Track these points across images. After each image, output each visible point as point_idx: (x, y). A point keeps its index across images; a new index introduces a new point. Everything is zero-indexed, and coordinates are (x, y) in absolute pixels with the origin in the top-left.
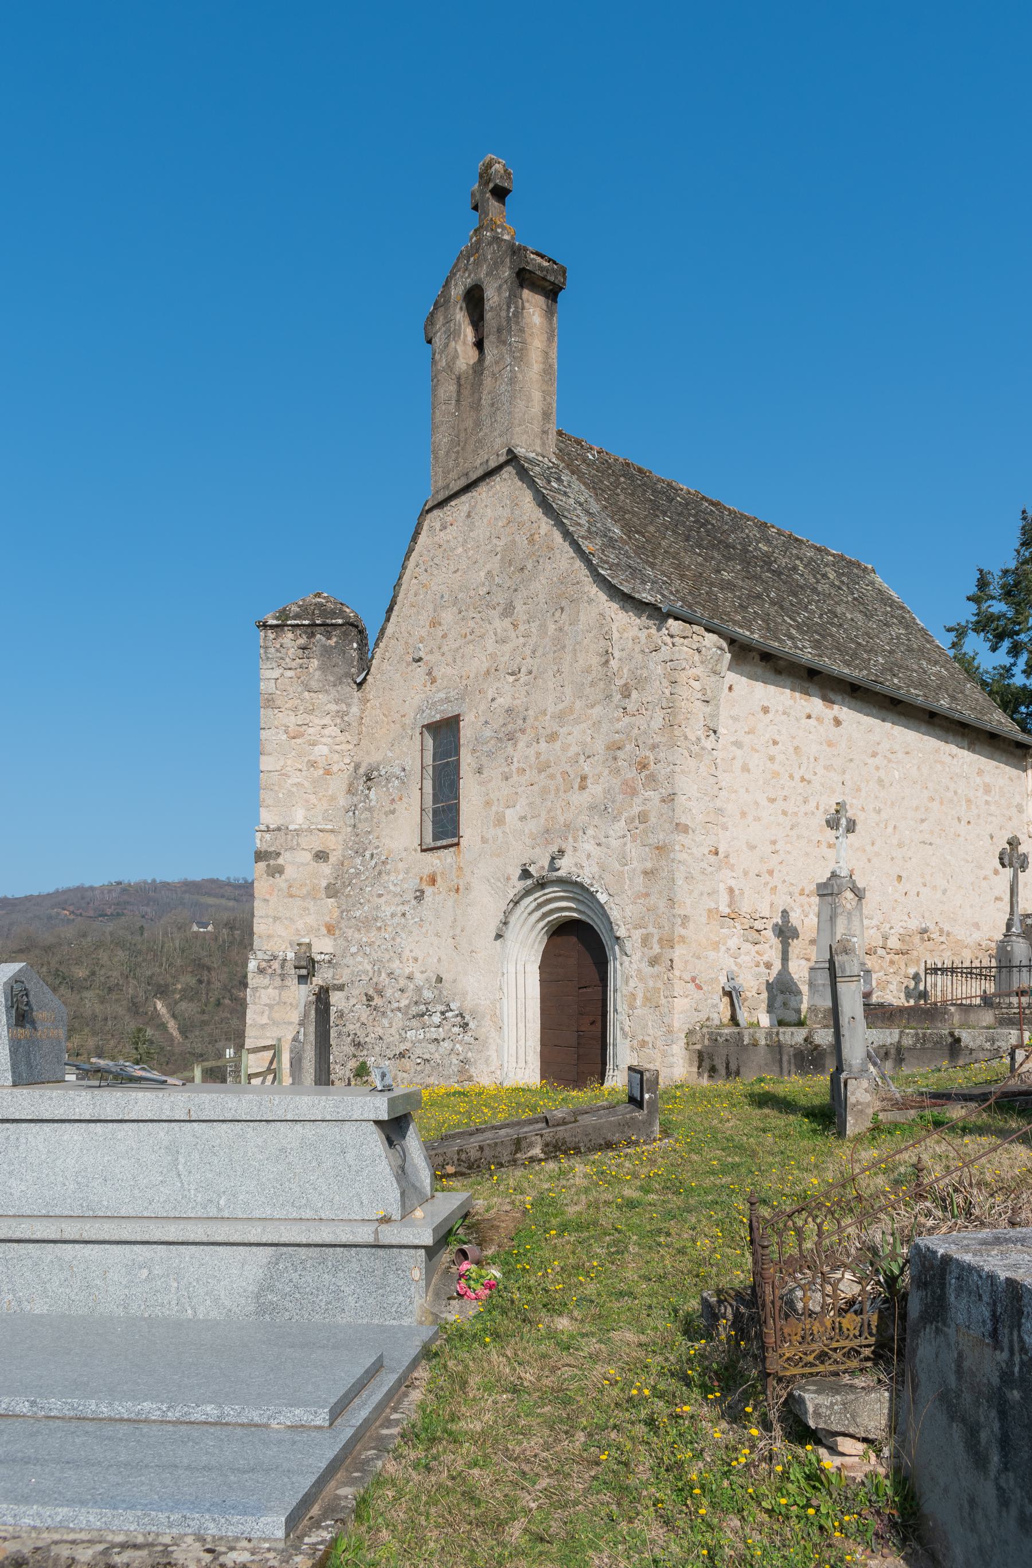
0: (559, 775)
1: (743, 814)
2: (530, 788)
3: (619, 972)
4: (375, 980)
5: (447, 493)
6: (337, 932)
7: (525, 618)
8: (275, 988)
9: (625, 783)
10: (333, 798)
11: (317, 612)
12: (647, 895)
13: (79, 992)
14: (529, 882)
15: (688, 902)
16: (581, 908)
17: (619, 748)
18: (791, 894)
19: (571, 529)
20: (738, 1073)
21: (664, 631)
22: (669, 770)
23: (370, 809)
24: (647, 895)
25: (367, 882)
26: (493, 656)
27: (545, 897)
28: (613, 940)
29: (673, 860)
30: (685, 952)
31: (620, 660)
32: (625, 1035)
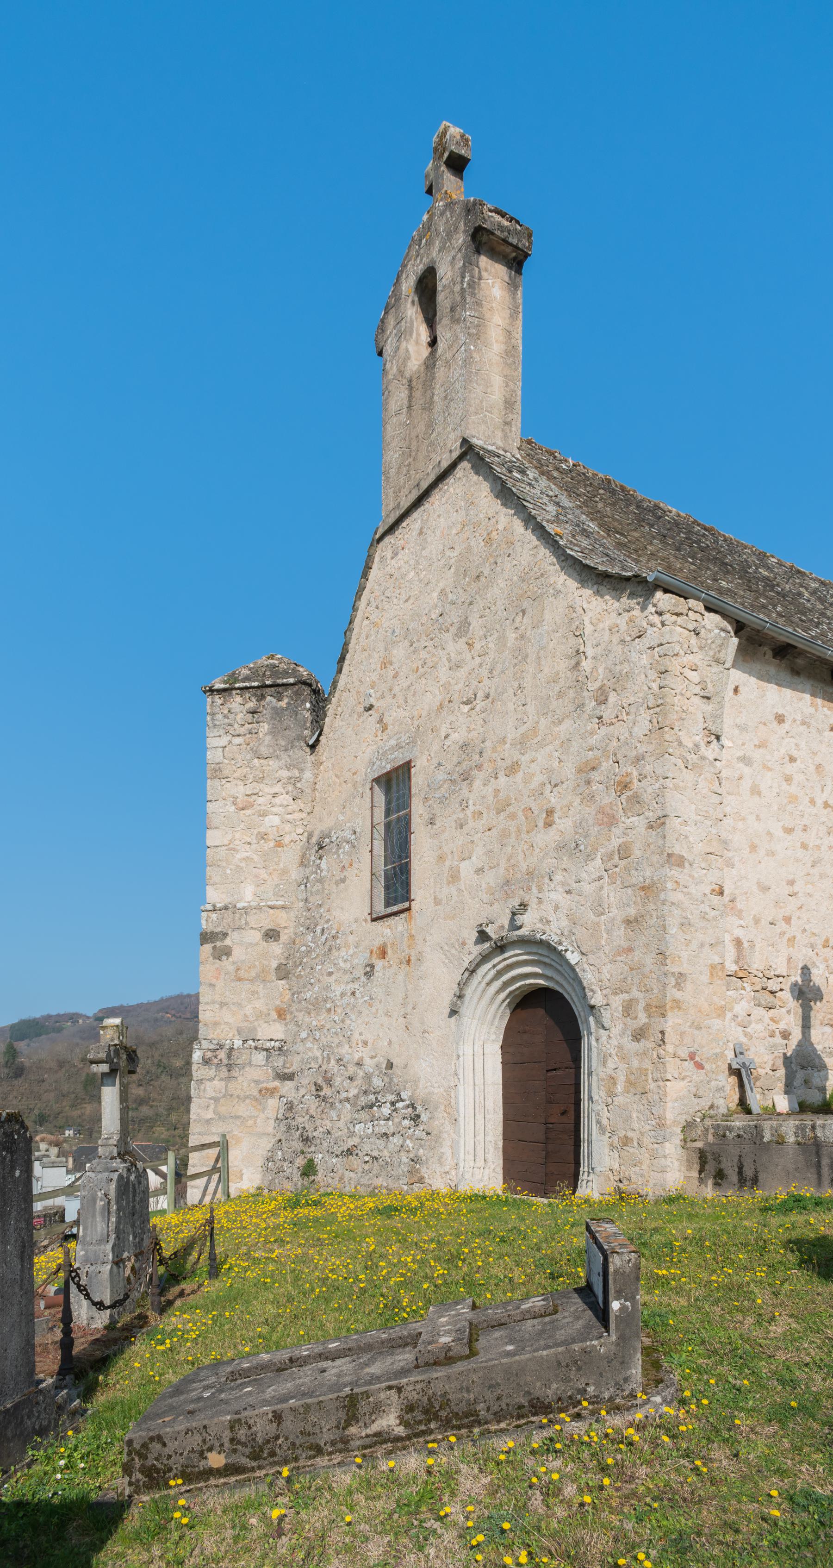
0: (520, 814)
1: (753, 848)
2: (487, 834)
3: (594, 1050)
4: (324, 1067)
5: (398, 513)
6: (288, 1017)
7: (481, 633)
8: (221, 1079)
9: (601, 811)
10: (285, 872)
11: (268, 673)
12: (630, 950)
13: (177, 1078)
14: (487, 945)
15: (685, 955)
16: (549, 973)
17: (593, 769)
18: (813, 947)
19: (533, 512)
20: (755, 1181)
21: (651, 609)
22: (657, 786)
23: (321, 881)
24: (630, 950)
25: (317, 961)
26: (446, 687)
27: (505, 963)
28: (587, 1009)
29: (664, 903)
30: (680, 1021)
31: (594, 658)
32: (602, 1130)
